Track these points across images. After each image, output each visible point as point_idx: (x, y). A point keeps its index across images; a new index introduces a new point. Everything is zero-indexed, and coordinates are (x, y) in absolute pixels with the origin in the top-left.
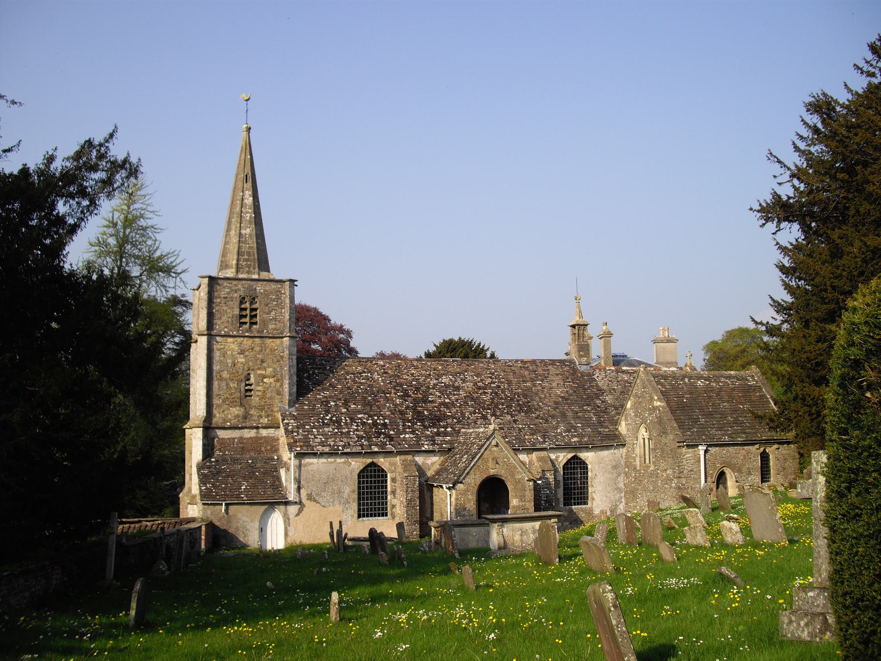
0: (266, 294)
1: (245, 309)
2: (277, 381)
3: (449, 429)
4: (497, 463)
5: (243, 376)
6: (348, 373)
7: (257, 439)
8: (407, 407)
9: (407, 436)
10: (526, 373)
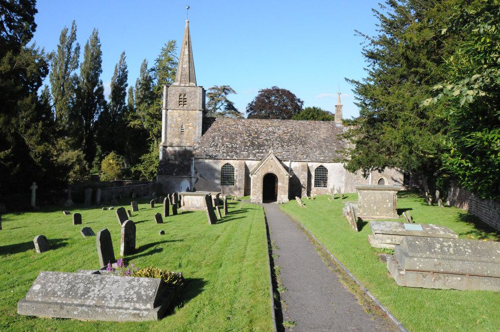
0: (190, 93)
6: (227, 125)
8: (249, 140)
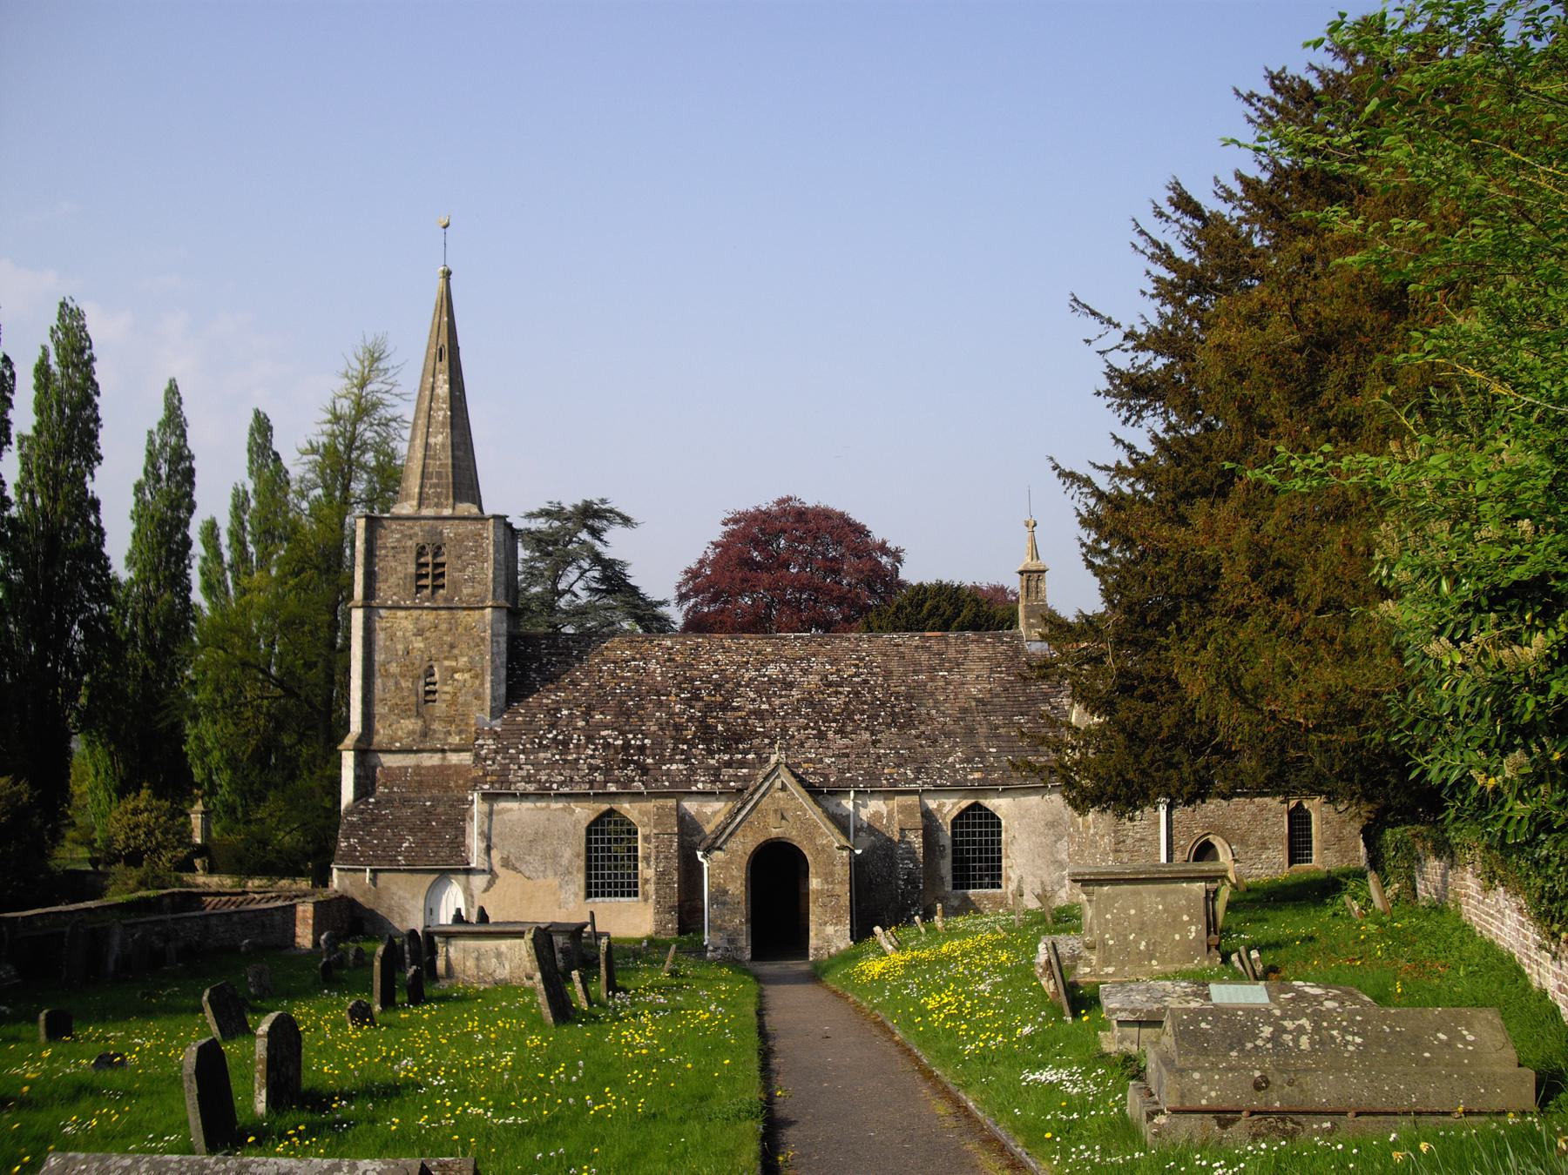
0: (459, 540)
1: (426, 565)
2: (476, 676)
3: (750, 756)
4: (783, 817)
5: (421, 671)
6: (605, 662)
7: (442, 769)
9: (674, 767)
10: (925, 657)
